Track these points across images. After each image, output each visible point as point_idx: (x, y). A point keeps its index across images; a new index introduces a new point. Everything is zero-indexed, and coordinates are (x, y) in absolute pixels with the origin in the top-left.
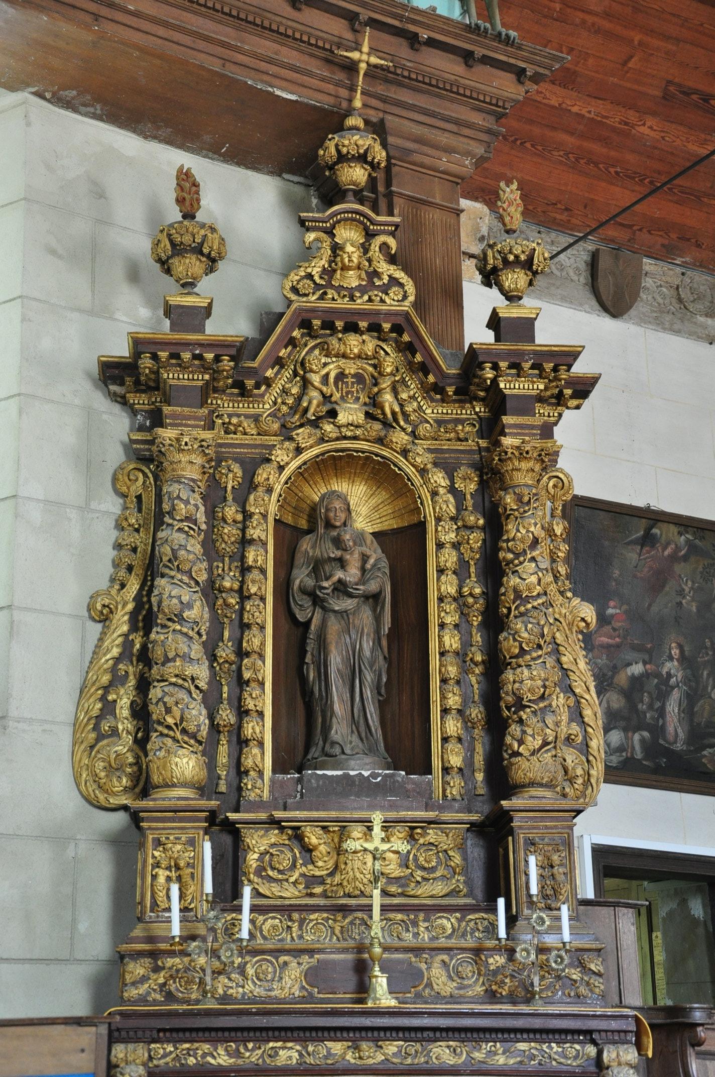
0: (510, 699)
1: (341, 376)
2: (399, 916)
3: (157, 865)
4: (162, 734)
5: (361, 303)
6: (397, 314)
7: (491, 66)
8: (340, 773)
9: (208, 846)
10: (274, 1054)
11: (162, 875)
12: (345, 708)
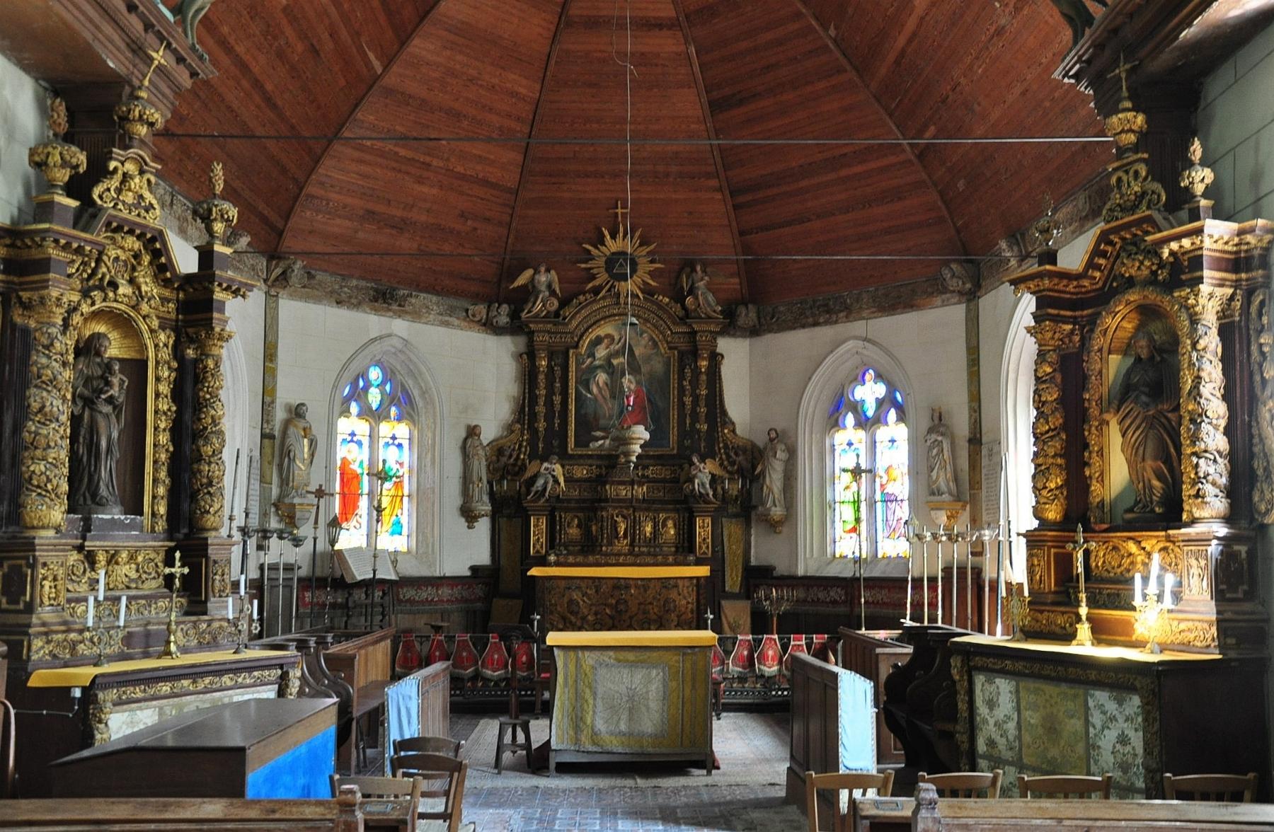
0: (205, 481)
1: (117, 259)
2: (144, 602)
3: (44, 578)
4: (39, 494)
5: (132, 217)
6: (156, 230)
7: (877, 714)
8: (109, 517)
9: (1100, 779)
10: (231, 696)
11: (47, 584)
12: (107, 472)
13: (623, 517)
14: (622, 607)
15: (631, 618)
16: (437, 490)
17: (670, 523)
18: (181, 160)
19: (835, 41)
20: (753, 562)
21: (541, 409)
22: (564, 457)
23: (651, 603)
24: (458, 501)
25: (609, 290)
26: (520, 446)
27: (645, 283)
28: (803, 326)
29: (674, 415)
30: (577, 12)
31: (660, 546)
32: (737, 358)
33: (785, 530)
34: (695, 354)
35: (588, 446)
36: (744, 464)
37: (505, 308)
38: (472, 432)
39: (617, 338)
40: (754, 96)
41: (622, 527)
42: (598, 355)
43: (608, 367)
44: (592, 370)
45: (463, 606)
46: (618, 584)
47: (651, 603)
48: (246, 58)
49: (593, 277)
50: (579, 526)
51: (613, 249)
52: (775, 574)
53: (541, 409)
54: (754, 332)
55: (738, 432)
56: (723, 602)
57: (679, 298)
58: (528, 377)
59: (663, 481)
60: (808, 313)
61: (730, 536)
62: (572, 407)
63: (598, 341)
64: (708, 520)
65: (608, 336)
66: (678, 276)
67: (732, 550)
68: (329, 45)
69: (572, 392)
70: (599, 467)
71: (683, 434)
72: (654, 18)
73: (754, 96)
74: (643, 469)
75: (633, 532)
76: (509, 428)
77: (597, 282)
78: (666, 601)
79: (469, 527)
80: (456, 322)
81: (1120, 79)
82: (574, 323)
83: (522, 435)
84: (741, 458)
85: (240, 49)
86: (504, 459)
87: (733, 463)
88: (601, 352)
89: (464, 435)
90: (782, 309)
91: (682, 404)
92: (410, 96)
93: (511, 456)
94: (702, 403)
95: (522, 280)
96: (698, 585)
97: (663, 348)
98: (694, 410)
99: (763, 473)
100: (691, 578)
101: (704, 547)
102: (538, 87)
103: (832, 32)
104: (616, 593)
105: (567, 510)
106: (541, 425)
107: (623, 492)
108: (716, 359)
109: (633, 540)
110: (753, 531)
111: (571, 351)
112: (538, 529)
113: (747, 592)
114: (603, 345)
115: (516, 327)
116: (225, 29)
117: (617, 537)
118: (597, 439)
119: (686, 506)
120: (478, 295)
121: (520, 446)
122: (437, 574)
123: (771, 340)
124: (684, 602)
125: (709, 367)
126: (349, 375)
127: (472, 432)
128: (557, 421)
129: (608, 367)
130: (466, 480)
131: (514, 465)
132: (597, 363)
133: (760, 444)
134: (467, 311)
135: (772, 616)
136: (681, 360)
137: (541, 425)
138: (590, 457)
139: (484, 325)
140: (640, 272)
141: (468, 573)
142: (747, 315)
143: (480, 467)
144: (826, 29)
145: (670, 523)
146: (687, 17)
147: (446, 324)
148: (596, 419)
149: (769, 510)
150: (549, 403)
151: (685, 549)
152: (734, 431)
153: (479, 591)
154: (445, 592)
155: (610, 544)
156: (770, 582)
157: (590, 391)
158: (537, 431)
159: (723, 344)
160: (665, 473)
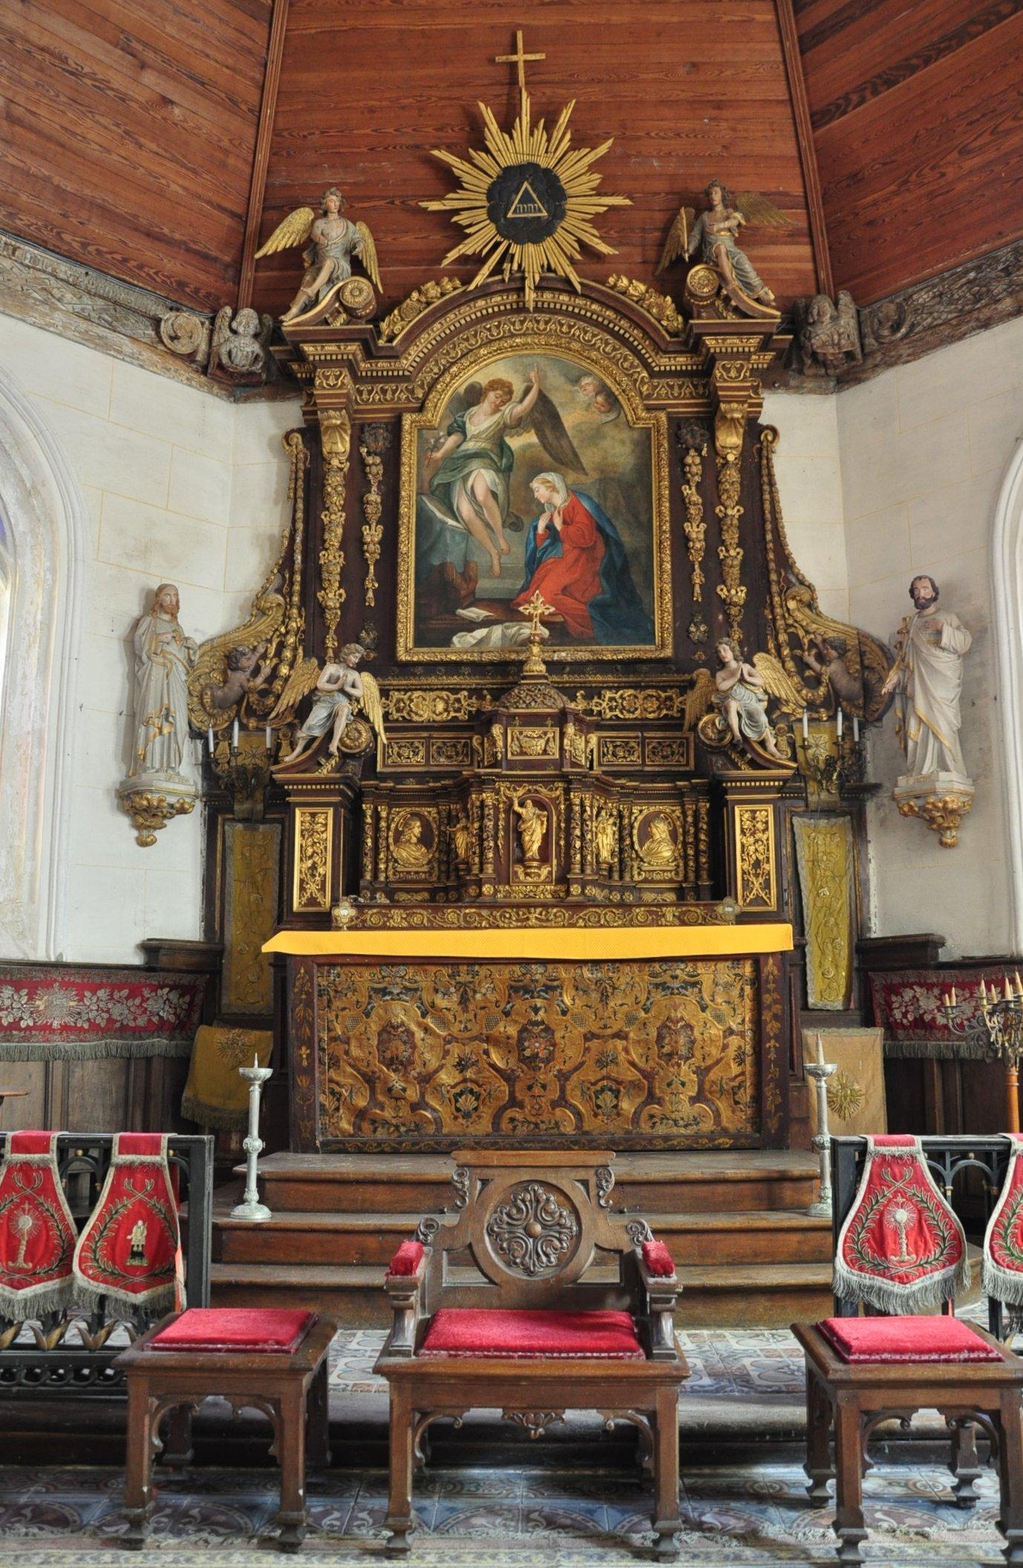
13: (539, 804)
14: (537, 1046)
15: (563, 1077)
16: (50, 737)
17: (660, 830)
20: (877, 929)
21: (332, 559)
22: (383, 663)
23: (620, 1035)
24: (112, 773)
25: (498, 270)
26: (281, 646)
27: (584, 247)
28: (986, 324)
29: (664, 563)
31: (634, 889)
32: (806, 434)
33: (967, 835)
34: (709, 418)
35: (447, 642)
36: (844, 683)
37: (248, 319)
38: (159, 603)
39: (518, 387)
41: (534, 841)
42: (472, 429)
43: (499, 454)
44: (459, 462)
45: (115, 1042)
46: (527, 979)
47: (620, 1035)
49: (460, 234)
50: (425, 840)
51: (508, 159)
52: (943, 956)
53: (332, 559)
54: (845, 372)
55: (822, 605)
56: (809, 1034)
57: (670, 277)
58: (308, 486)
59: (642, 725)
60: (998, 288)
61: (815, 862)
62: (408, 546)
63: (474, 396)
64: (766, 813)
65: (495, 385)
66: (668, 227)
67: (824, 896)
69: (408, 511)
70: (476, 692)
71: (685, 611)
74: (589, 697)
75: (564, 847)
76: (258, 608)
77: (468, 248)
78: (665, 1029)
79: (143, 843)
80: (128, 346)
82: (414, 353)
83: (286, 617)
84: (834, 668)
86: (239, 678)
87: (815, 682)
88: (481, 421)
89: (135, 609)
90: (923, 297)
91: (681, 541)
93: (256, 671)
94: (731, 536)
95: (280, 240)
96: (757, 982)
97: (633, 408)
98: (711, 551)
99: (904, 692)
100: (736, 959)
101: (757, 883)
104: (520, 1005)
105: (395, 799)
106: (333, 597)
107: (537, 743)
108: (759, 439)
109: (566, 868)
110: (872, 850)
111: (407, 419)
112: (314, 837)
113: (866, 1007)
114: (486, 406)
115: (280, 373)
117: (521, 860)
118: (471, 626)
119: (703, 778)
120: (181, 285)
121: (281, 646)
122: (40, 956)
123: (888, 385)
124: (716, 1031)
125: (744, 455)
126: (970, 1412)
127: (159, 603)
128: (371, 584)
129: (499, 454)
130: (134, 717)
131: (264, 693)
132: (470, 446)
133: (882, 630)
134: (156, 322)
135: (1003, 1063)
136: (675, 438)
137: (333, 597)
138: (454, 667)
139: (204, 370)
140: (571, 221)
141: (137, 960)
142: (835, 319)
143: (173, 690)
145: (660, 830)
147: (102, 345)
148: (468, 576)
149: (931, 778)
150: (353, 542)
151: (707, 880)
152: (811, 605)
153: (160, 1005)
154: (57, 1005)
155: (504, 877)
156: (932, 977)
157: (452, 511)
158: (322, 609)
159: (777, 408)
160: (642, 705)
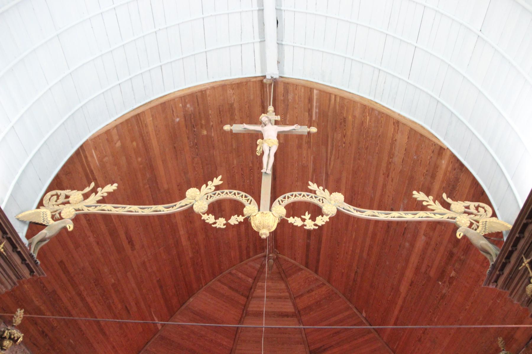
18: (48, 349)
19: (365, 318)
30: (251, 309)
40: (330, 347)
48: (92, 305)
68: (134, 309)
72: (285, 312)
73: (330, 347)
81: (527, 268)
85: (89, 300)
92: (173, 342)
102: (232, 342)
103: (364, 314)
116: (82, 288)
144: (361, 313)
146: (299, 312)
